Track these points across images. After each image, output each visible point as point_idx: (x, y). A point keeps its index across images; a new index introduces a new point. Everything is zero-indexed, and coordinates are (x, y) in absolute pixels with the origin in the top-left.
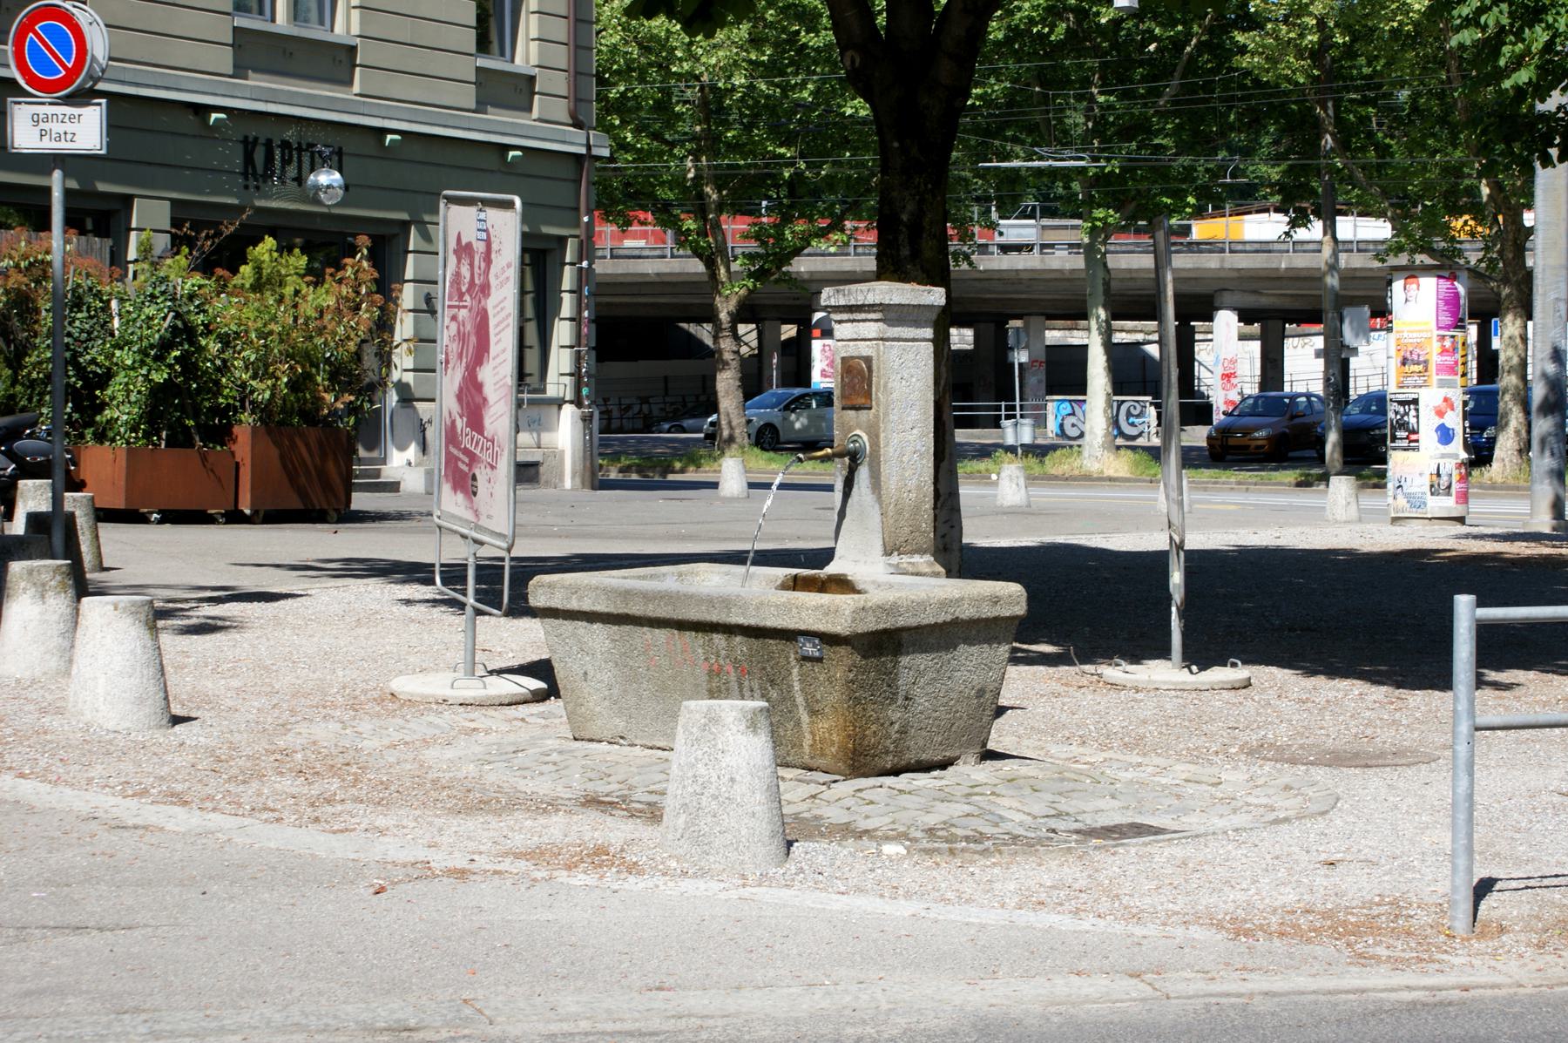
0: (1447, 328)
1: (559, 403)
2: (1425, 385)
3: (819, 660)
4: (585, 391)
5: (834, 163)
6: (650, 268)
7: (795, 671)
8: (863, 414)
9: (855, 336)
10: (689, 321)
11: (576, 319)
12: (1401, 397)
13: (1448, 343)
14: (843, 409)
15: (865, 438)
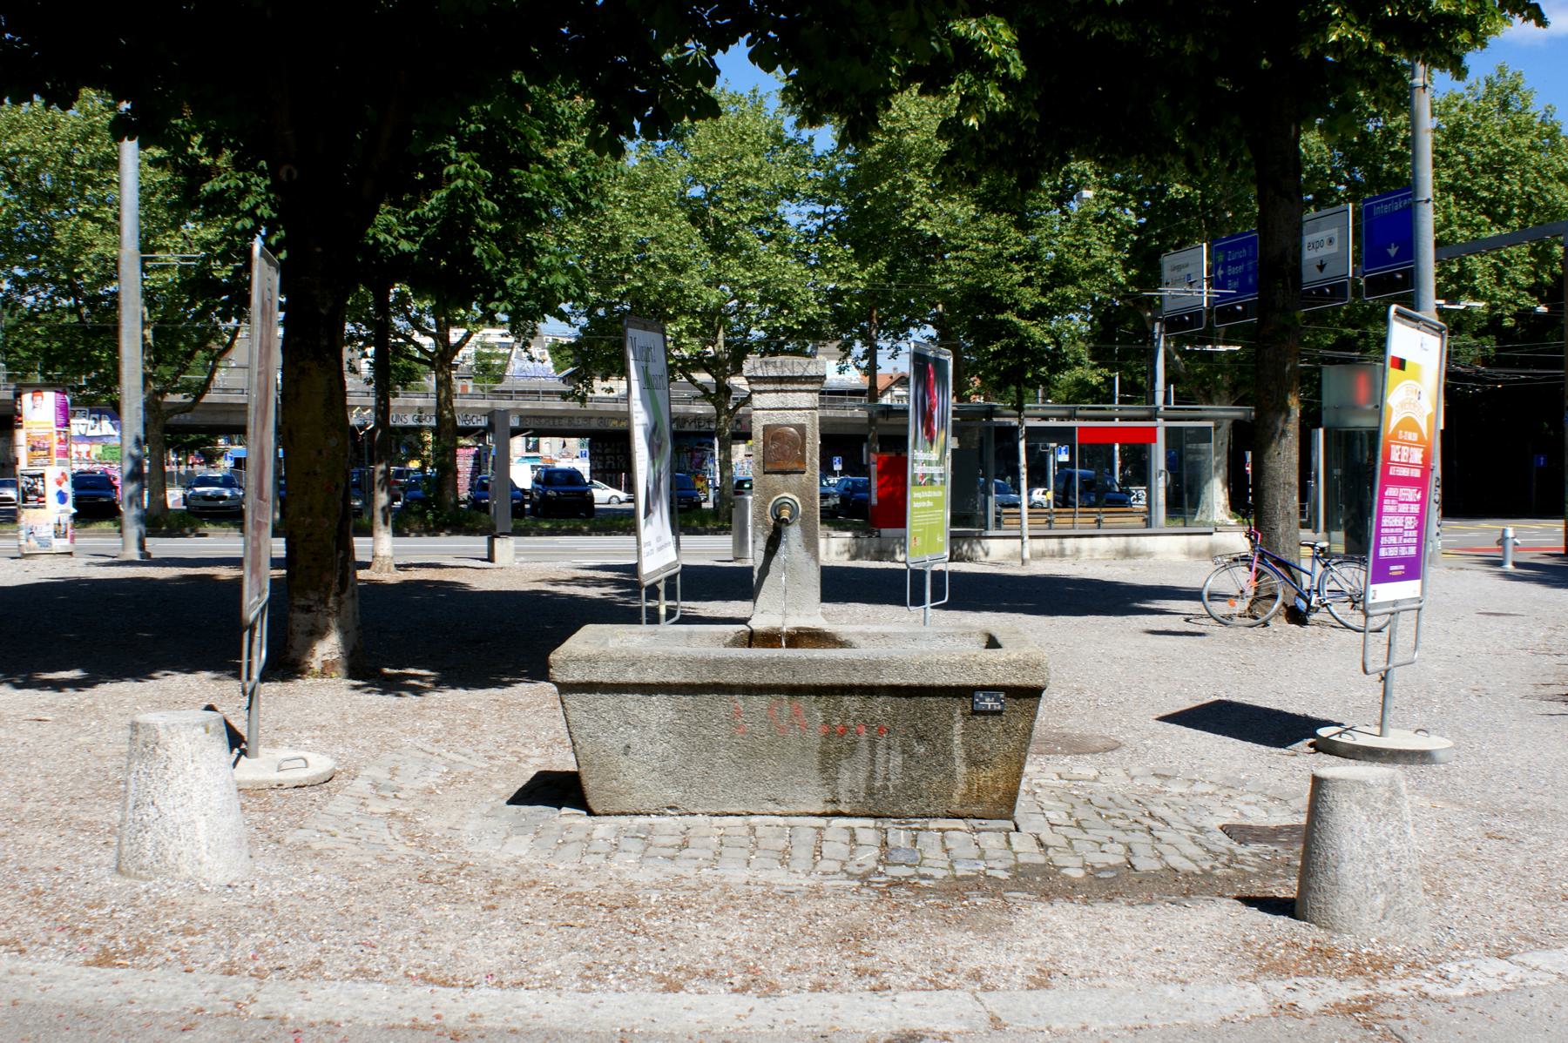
0: (62, 426)
2: (49, 464)
3: (999, 713)
7: (958, 727)
8: (793, 479)
9: (781, 406)
12: (31, 473)
13: (62, 437)
15: (797, 500)
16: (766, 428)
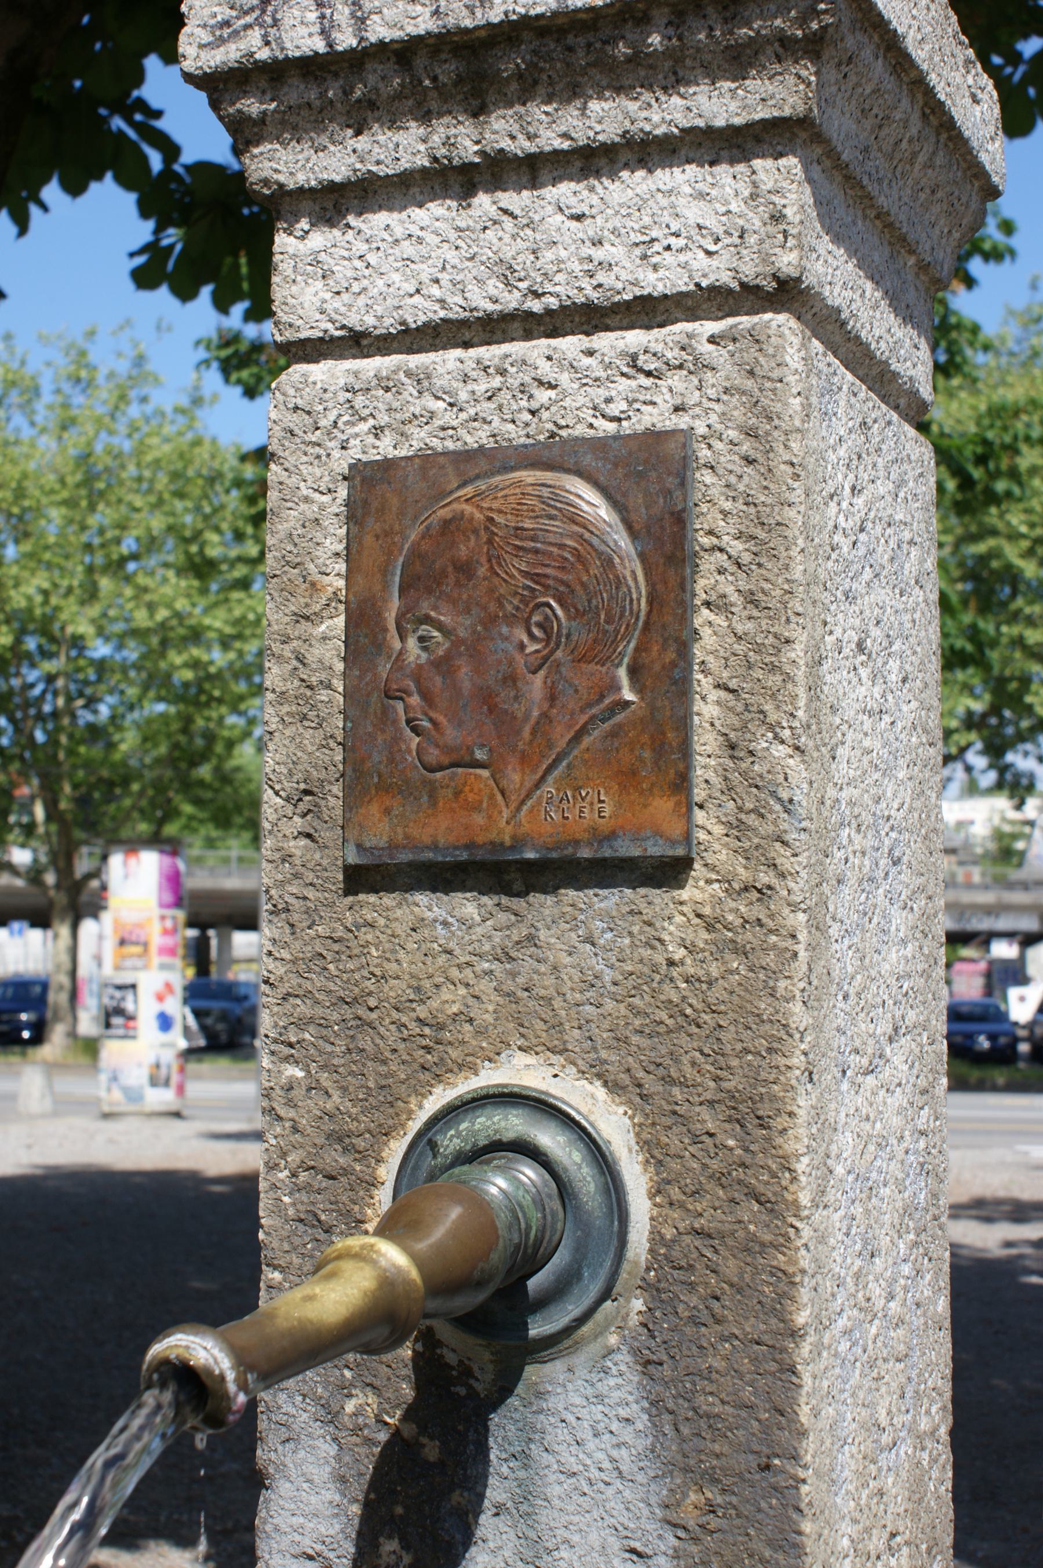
2: (146, 967)
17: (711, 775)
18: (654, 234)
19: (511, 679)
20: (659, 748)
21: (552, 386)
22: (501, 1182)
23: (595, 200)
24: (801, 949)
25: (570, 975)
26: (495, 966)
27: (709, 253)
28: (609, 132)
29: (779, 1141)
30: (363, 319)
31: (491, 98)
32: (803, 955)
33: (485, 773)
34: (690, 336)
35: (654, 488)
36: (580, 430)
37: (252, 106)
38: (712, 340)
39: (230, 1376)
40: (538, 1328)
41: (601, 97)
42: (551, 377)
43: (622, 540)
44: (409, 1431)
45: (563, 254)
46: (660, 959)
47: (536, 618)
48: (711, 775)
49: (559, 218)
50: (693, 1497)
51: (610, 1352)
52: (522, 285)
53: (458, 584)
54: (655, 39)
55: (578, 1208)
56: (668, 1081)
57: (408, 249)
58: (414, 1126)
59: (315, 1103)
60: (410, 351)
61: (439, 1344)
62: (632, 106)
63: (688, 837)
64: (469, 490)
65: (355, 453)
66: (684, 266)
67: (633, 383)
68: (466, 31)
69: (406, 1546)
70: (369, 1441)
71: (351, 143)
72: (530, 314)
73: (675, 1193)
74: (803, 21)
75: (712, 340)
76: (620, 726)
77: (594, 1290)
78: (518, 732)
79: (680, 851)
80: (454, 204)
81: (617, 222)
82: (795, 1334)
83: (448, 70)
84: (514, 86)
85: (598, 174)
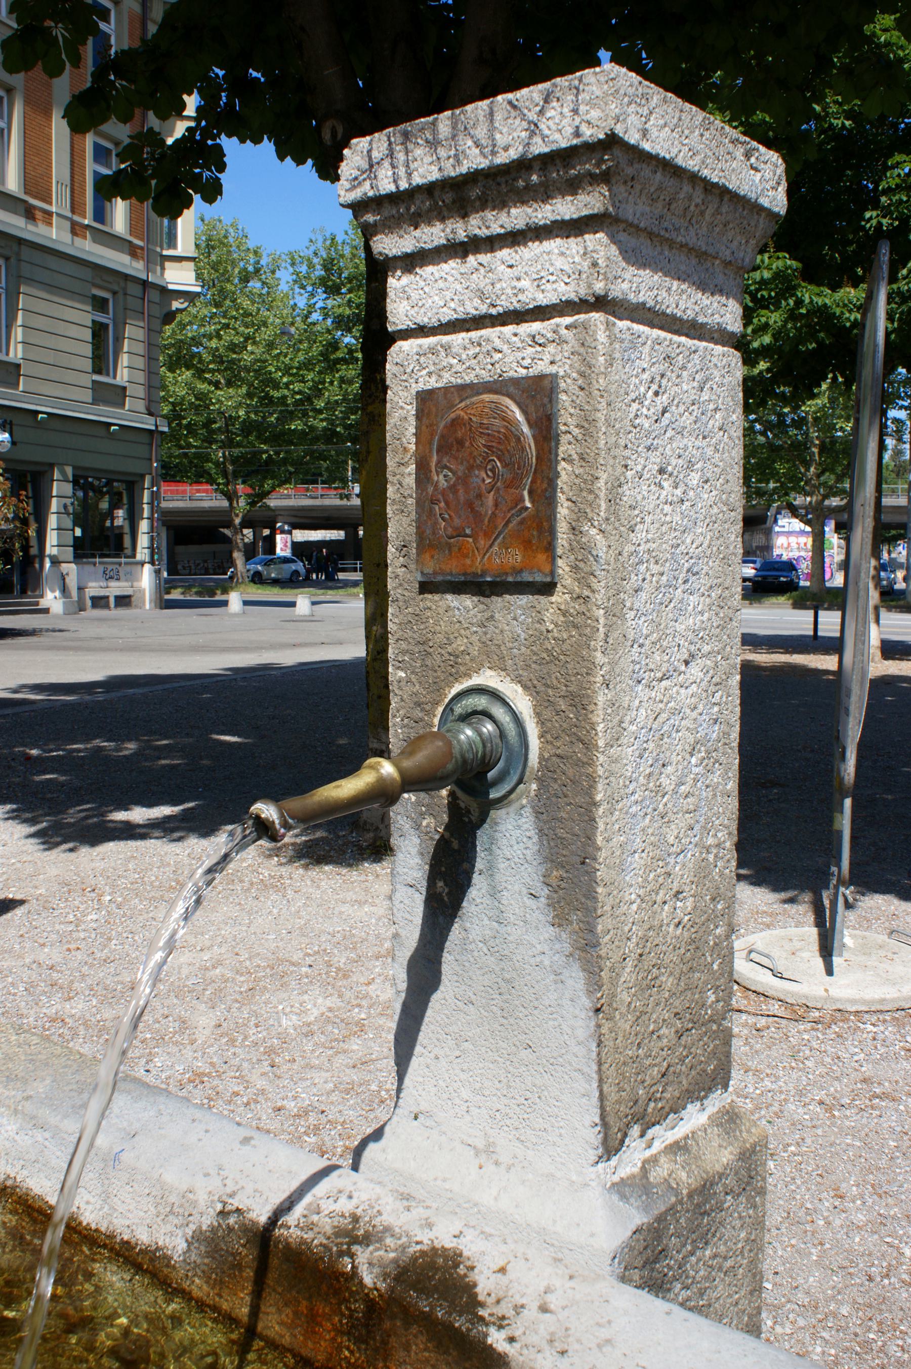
1: (142, 564)
4: (156, 557)
5: (286, 452)
6: (206, 504)
9: (474, 307)
10: (224, 527)
11: (151, 518)
14: (426, 587)
15: (523, 704)
16: (425, 398)
17: (564, 543)
18: (542, 274)
19: (479, 496)
20: (540, 528)
21: (500, 352)
22: (469, 732)
23: (518, 257)
24: (601, 627)
25: (508, 634)
26: (478, 629)
27: (566, 284)
28: (520, 224)
29: (590, 716)
30: (424, 320)
31: (469, 209)
32: (601, 629)
33: (471, 540)
34: (558, 326)
35: (539, 403)
36: (512, 374)
37: (370, 218)
38: (567, 328)
39: (277, 822)
40: (494, 795)
41: (515, 207)
42: (499, 347)
43: (526, 429)
44: (447, 835)
45: (504, 285)
46: (543, 629)
47: (489, 467)
48: (564, 543)
49: (503, 267)
50: (555, 873)
51: (523, 807)
52: (488, 301)
53: (458, 450)
54: (534, 178)
55: (507, 742)
56: (547, 686)
57: (441, 284)
58: (447, 700)
59: (409, 689)
60: (445, 334)
61: (457, 798)
62: (529, 210)
63: (552, 573)
64: (462, 405)
65: (421, 386)
66: (555, 290)
67: (533, 350)
68: (452, 178)
69: (446, 885)
70: (432, 839)
71: (413, 233)
72: (491, 316)
73: (549, 737)
74: (598, 165)
75: (567, 328)
76: (524, 519)
77: (515, 779)
78: (482, 521)
79: (548, 579)
80: (459, 261)
81: (526, 269)
82: (595, 804)
83: (449, 197)
84: (478, 203)
85: (519, 244)
